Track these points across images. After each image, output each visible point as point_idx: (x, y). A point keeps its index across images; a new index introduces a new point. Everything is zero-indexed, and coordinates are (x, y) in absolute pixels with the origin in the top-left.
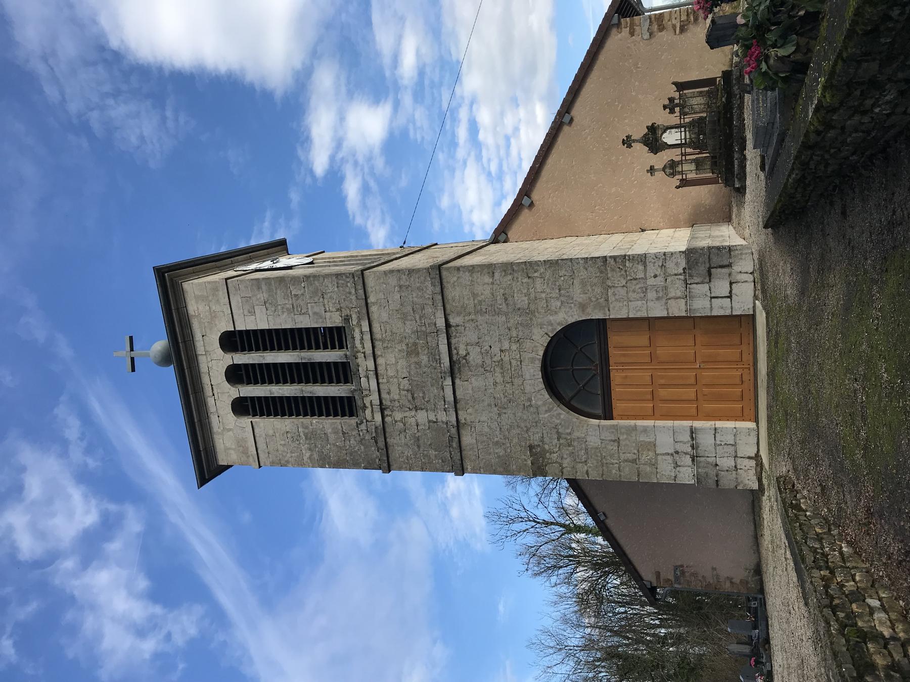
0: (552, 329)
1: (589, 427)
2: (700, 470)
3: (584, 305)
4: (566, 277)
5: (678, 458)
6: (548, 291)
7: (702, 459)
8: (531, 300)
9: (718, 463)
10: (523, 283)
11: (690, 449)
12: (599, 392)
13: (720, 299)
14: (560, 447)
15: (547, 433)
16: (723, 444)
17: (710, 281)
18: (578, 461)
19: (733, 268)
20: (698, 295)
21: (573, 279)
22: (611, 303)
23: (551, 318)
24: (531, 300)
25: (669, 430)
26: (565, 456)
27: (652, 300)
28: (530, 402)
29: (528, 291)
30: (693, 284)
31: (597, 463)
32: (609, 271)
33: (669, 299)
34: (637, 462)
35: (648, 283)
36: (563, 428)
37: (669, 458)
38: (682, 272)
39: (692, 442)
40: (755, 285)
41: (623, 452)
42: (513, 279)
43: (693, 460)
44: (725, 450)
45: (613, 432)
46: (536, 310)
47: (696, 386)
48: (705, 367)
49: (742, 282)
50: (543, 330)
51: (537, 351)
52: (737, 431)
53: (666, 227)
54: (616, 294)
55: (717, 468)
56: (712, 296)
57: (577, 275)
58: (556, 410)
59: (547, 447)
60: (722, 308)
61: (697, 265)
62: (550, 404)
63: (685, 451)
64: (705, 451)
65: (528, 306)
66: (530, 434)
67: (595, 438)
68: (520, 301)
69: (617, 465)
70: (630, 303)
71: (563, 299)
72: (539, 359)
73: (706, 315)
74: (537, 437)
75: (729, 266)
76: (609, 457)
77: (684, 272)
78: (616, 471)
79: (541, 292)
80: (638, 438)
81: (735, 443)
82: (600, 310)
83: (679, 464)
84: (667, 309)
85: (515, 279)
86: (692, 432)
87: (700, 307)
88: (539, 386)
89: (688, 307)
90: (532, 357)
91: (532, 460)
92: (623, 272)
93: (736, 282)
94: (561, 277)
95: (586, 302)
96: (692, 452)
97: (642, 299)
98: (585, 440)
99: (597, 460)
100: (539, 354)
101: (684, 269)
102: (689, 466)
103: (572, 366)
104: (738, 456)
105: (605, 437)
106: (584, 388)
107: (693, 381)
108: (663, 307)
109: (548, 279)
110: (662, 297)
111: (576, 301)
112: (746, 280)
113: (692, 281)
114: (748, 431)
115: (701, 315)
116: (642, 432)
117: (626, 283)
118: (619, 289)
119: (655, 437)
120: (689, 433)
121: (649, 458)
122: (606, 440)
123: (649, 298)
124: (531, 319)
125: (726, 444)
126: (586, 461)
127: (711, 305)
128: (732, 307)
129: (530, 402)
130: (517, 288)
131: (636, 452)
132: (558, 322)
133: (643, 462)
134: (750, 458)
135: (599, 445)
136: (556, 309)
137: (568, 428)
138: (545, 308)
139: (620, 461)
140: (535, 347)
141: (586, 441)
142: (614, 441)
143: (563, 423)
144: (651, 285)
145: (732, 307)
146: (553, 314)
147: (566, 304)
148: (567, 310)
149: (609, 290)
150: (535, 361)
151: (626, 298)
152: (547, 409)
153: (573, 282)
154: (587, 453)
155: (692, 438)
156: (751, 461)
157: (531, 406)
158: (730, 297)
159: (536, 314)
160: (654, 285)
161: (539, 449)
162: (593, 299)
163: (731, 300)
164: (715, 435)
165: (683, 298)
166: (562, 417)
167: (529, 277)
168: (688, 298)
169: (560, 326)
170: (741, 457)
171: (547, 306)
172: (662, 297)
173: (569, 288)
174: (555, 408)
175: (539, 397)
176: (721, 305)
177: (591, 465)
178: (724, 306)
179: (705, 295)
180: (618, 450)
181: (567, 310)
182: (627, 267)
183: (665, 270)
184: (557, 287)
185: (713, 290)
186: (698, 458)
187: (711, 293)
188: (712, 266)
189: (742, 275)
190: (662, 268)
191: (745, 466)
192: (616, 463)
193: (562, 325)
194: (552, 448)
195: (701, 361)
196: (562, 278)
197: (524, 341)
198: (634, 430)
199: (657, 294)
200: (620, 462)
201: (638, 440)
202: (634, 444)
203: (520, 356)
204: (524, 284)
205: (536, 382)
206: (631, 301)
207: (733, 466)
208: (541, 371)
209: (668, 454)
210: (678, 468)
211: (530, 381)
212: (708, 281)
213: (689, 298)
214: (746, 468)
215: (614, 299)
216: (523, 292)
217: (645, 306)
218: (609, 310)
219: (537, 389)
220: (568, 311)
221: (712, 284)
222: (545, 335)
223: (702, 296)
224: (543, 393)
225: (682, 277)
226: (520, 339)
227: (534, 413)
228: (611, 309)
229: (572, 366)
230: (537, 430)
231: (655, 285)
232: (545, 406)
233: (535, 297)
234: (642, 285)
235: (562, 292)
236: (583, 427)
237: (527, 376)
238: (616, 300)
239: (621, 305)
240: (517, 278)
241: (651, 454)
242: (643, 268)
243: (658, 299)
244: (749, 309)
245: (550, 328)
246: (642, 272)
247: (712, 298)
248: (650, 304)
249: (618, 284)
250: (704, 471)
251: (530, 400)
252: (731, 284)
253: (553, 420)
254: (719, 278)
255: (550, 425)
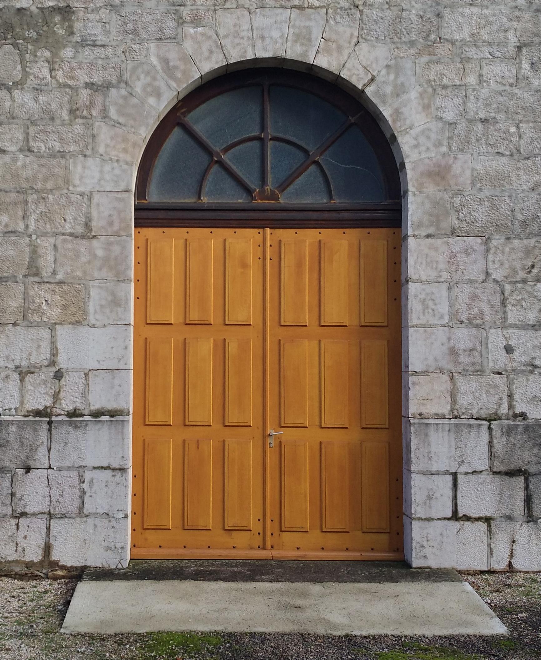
0: (385, 95)
1: (125, 167)
2: (13, 428)
3: (443, 178)
4: (515, 139)
5: (43, 377)
6: (484, 92)
7: (43, 435)
8: (461, 47)
9: (33, 473)
10: (506, 31)
11: (67, 405)
12: (205, 199)
13: (450, 493)
14: (69, 87)
15: (107, 58)
16: (85, 486)
17: (495, 473)
18: (32, 130)
19: (525, 525)
20: (462, 445)
21: (512, 155)
22: (448, 244)
23: (413, 95)
24: (461, 47)
25: (119, 360)
26: (43, 98)
27: (449, 339)
28: (192, 22)
29: (484, 41)
30: (490, 434)
31: (27, 179)
32: (526, 242)
33: (452, 378)
34: (32, 279)
35: (493, 331)
36: (121, 101)
37: (44, 356)
38: (517, 411)
39: (86, 412)
40: (482, 572)
41: (59, 247)
42: (516, 7)
43: (38, 413)
44: (68, 490)
45: (111, 224)
46: (434, 58)
47: (220, 426)
48: (268, 450)
49: (489, 545)
50: (384, 72)
51: (328, 51)
52: (117, 520)
53: (407, 354)
54: (468, 254)
55: (21, 472)
56: (461, 479)
57: (520, 165)
58: (169, 86)
59: (67, 53)
60: (429, 498)
61: (534, 445)
62: (184, 72)
63: (62, 395)
64: (66, 444)
65: (447, 40)
66: (104, 14)
67: (96, 181)
68: (460, 20)
69: (21, 227)
70: (445, 286)
71: (462, 127)
72: (305, 54)
73: (414, 460)
74: (96, 31)
75: (530, 518)
76: (42, 208)
77: (515, 416)
78: (6, 225)
79: (481, 75)
80: (96, 283)
81: (87, 516)
82: (430, 215)
83: (29, 378)
84: (426, 372)
85: (518, 13)
86: (113, 414)
87: (433, 449)
88: (234, 47)
89: (431, 421)
90: (313, 36)
91: (31, 12)
92: (522, 274)
93: (490, 531)
94: (518, 127)
95: (452, 182)
96: (59, 412)
97: (454, 314)
98: (88, 153)
99: (35, 177)
100: (319, 55)
101: (523, 416)
102: (22, 403)
103: (274, 139)
104: (52, 521)
105: (98, 205)
106: (217, 162)
107: (233, 417)
108: (431, 361)
109: (512, 96)
110: (456, 362)
111: (455, 158)
112: (494, 554)
113: (497, 433)
114: (118, 545)
115: (413, 448)
116: (113, 294)
117: (495, 281)
118: (481, 265)
119: (98, 324)
120: (111, 405)
121: (44, 307)
122: (89, 206)
123: (456, 331)
124: (412, 43)
125: (84, 493)
126: (30, 150)
127: (438, 473)
128: (433, 519)
129: (192, 22)
130: (494, 15)
131: (60, 276)
132: (404, 110)
133: (31, 293)
134: (48, 549)
135: (75, 186)
136: (437, 109)
137: (120, 112)
138: (441, 79)
139: (34, 237)
140: (340, 49)
141: (85, 156)
142: (87, 225)
143: (135, 101)
144: (487, 338)
145: (433, 519)
146: (423, 99)
147: (447, 134)
148: (433, 136)
149: (479, 240)
150: (302, 45)
151: (457, 277)
152: (171, 64)
153: (503, 155)
154: (53, 156)
155: (97, 414)
156: (40, 552)
157: (181, 22)
158: (455, 516)
159: (425, 59)
160: (487, 344)
161: (61, 32)
162: (457, 201)
163: (449, 519)
164: (108, 468)
165: (452, 410)
166: (152, 101)
167: (519, 48)
168: (453, 421)
169: (391, 116)
170: (48, 529)
171: (445, 87)
172: (456, 362)
173: (488, 144)
174: (173, 84)
175: (205, 47)
176: (437, 495)
177: (19, 163)
178: (433, 502)
179: (463, 462)
180: (63, 234)
181: (433, 136)
182: (534, 285)
183: (523, 371)
184: (493, 115)
185: (472, 478)
186: (45, 426)
187: (467, 473)
188: (531, 479)
189: (508, 546)
190: (528, 365)
191: (25, 537)
192: (27, 226)
193: (394, 121)
194: (66, 66)
195: (283, 439)
196: (513, 130)
197: (354, 20)
198: (117, 274)
199: (464, 350)
200: (30, 236)
201: (91, 283)
202: (79, 274)
203: (316, 8)
204: (501, 35)
205: (245, 42)
206: (450, 289)
207: (25, 507)
208: (275, 59)
209: (54, 353)
210: (16, 376)
211: (246, 27)
212: (494, 470)
213: (456, 425)
214: (20, 539)
215: (456, 248)
216: (482, 32)
217: (436, 322)
218: (428, 236)
219: (226, 42)
220: (428, 138)
221: (487, 478)
222: (370, 77)
223: (459, 454)
224: (214, 58)
225: (504, 410)
226: (361, 12)
227: (161, 30)
228: (430, 240)
229: (274, 139)
230: (114, 32)
231: (487, 348)
232: (180, 59)
233: (468, 60)
234: (488, 318)
235: (480, 126)
236: (125, 151)
237: (260, 20)
238: (453, 256)
239: (442, 266)
240: (518, 19)
241: (54, 313)
242: (531, 323)
243: (453, 352)
244: (425, 557)
245: (388, 89)
246: (521, 318)
247: (455, 475)
248: (441, 334)
249: (494, 262)
250: (12, 439)
251: (197, 21)
252: (488, 520)
253: (142, 76)
254: (501, 494)
255: (129, 67)
